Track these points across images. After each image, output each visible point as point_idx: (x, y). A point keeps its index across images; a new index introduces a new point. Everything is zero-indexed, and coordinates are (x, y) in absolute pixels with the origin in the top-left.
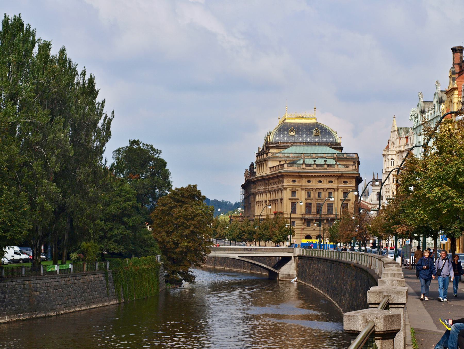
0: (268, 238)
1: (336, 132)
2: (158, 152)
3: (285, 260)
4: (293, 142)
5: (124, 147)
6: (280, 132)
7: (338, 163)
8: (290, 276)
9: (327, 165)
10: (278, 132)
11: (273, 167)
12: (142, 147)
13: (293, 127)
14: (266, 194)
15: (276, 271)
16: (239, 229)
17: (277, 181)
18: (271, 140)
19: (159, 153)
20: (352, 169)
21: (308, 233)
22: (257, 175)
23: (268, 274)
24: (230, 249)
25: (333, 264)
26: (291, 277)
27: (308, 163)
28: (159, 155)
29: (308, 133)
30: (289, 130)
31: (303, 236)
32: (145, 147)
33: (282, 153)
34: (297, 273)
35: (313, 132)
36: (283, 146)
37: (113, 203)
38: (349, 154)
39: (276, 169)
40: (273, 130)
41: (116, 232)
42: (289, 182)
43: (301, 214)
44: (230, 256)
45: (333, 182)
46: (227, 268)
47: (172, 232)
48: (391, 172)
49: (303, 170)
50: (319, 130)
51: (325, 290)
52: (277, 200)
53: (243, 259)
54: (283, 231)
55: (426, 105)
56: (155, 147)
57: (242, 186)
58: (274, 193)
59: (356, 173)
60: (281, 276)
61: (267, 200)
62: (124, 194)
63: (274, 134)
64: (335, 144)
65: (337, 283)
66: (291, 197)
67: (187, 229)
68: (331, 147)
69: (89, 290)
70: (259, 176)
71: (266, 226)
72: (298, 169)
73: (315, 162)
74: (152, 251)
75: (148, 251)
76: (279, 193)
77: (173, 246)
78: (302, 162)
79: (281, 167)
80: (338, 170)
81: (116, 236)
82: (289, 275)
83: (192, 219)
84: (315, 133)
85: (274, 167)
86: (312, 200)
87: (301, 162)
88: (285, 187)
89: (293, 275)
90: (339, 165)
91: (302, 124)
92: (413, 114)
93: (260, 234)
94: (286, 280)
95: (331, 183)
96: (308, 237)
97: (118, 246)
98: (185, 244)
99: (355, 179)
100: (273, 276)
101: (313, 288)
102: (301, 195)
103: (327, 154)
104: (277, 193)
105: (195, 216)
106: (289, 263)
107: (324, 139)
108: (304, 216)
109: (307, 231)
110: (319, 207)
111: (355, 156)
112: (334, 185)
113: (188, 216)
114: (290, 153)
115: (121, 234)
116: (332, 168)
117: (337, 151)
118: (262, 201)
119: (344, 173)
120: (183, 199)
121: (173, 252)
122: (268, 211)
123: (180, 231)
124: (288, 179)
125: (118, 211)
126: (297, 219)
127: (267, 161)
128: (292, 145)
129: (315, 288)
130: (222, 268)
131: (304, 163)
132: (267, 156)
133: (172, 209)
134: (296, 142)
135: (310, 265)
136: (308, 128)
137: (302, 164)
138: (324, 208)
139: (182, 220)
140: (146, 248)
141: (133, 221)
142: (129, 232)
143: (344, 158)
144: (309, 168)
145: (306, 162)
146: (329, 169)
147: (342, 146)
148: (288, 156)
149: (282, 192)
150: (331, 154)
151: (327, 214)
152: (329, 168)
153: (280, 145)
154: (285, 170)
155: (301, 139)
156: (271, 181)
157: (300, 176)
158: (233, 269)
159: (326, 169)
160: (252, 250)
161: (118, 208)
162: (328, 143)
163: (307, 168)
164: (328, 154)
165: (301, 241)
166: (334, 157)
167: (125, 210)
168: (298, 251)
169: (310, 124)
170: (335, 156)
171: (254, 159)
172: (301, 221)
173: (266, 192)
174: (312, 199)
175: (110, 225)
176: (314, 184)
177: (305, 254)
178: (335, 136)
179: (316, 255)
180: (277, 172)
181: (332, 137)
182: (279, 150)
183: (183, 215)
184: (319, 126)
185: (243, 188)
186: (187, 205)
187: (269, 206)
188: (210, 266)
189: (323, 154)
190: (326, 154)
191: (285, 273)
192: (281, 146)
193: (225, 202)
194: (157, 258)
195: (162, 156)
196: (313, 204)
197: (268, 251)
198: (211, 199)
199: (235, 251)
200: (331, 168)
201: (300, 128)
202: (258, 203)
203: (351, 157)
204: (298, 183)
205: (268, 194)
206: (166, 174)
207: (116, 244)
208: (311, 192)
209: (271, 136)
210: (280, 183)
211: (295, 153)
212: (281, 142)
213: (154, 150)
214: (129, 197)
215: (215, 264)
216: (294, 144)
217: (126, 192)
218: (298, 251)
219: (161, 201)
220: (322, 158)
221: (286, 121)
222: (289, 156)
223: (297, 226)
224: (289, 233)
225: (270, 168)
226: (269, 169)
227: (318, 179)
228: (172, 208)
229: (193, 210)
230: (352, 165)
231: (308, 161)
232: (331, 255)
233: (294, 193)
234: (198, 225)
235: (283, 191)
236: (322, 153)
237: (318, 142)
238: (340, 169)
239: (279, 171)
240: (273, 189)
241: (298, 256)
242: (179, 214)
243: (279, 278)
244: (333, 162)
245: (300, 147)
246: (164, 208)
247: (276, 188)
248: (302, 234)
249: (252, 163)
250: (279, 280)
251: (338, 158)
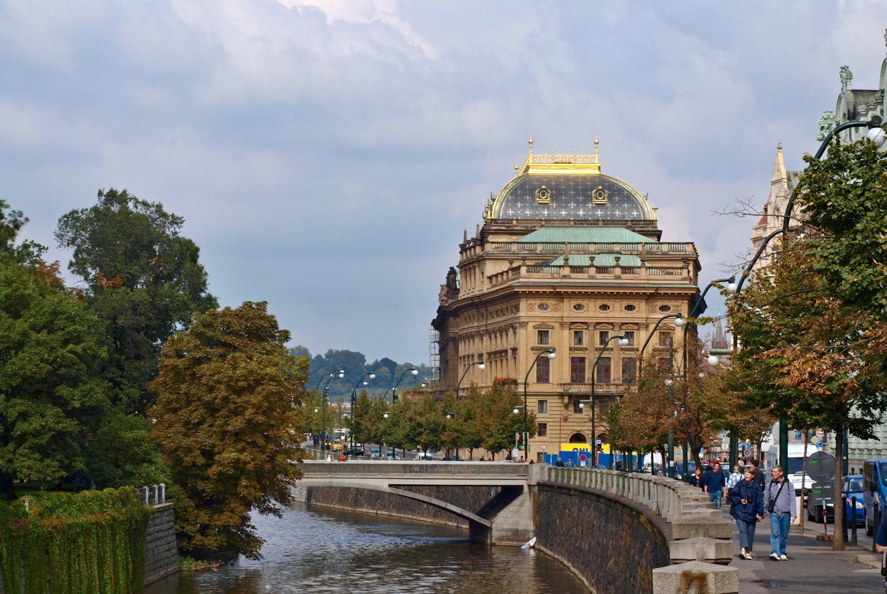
0: (473, 439)
2: (176, 221)
3: (510, 494)
4: (546, 220)
5: (86, 210)
6: (516, 198)
8: (519, 536)
9: (622, 268)
10: (510, 198)
11: (496, 276)
12: (134, 210)
13: (546, 185)
14: (482, 339)
15: (484, 522)
16: (411, 419)
17: (504, 306)
18: (496, 215)
19: (177, 224)
20: (679, 277)
21: (578, 428)
22: (462, 295)
23: (468, 527)
24: (369, 468)
25: (610, 509)
26: (522, 538)
27: (576, 264)
28: (177, 230)
29: (581, 198)
30: (537, 191)
31: (566, 436)
32: (141, 210)
33: (518, 243)
34: (536, 527)
35: (591, 196)
36: (523, 229)
37: (30, 347)
38: (673, 243)
39: (502, 278)
40: (501, 194)
41: (36, 423)
42: (532, 310)
43: (561, 384)
44: (368, 485)
45: (634, 307)
46: (384, 513)
47: (201, 423)
48: (768, 240)
49: (564, 280)
50: (606, 191)
51: (593, 578)
52: (506, 351)
53: (401, 492)
54: (507, 422)
55: (861, 99)
56: (168, 209)
58: (498, 335)
60: (495, 534)
61: (484, 352)
62: (60, 322)
64: (642, 223)
65: (616, 563)
66: (537, 345)
67: (236, 415)
68: (634, 231)
70: (466, 296)
71: (469, 411)
74: (145, 475)
75: (133, 474)
76: (509, 335)
77: (201, 460)
78: (562, 263)
80: (648, 280)
81: (36, 434)
82: (516, 532)
83: (251, 389)
84: (597, 199)
85: (499, 276)
86: (587, 352)
87: (560, 261)
88: (522, 320)
89: (526, 531)
90: (650, 268)
91: (567, 178)
92: (826, 125)
93: (457, 431)
94: (509, 543)
95: (631, 310)
96: (577, 438)
97: (41, 460)
98: (230, 455)
99: (688, 300)
100: (479, 532)
101: (568, 567)
102: (562, 339)
103: (623, 243)
104: (504, 334)
105: (258, 382)
106: (516, 502)
107: (617, 213)
108: (567, 387)
110: (603, 368)
111: (689, 248)
113: (240, 381)
114: (536, 243)
115: (50, 430)
116: (632, 275)
118: (473, 356)
119: (662, 286)
120: (229, 339)
121: (202, 477)
122: (486, 377)
123: (219, 422)
124: (529, 302)
125: (42, 368)
127: (482, 262)
128: (542, 226)
129: (572, 569)
130: (372, 511)
132: (483, 250)
133: (199, 365)
134: (553, 220)
135: (565, 508)
136: (580, 187)
137: (563, 266)
138: (614, 368)
139: (224, 393)
140: (129, 467)
141: (84, 396)
142: (73, 423)
143: (663, 253)
144: (580, 275)
145: (571, 263)
146: (627, 279)
147: (659, 229)
148: (531, 250)
149: (515, 332)
150: (632, 243)
151: (621, 382)
152: (625, 275)
154: (521, 280)
155: (563, 213)
156: (492, 309)
157: (558, 294)
158: (396, 515)
159: (619, 278)
160: (423, 469)
161: (42, 360)
162: (627, 221)
163: (574, 275)
164: (625, 243)
165: (560, 447)
166: (638, 251)
167: (61, 366)
168: (538, 474)
169: (584, 178)
170: (640, 247)
171: (455, 259)
172: (561, 401)
173: (482, 333)
174: (586, 349)
175: (20, 405)
176: (591, 311)
177: (553, 479)
178: (644, 206)
179: (577, 483)
180: (505, 285)
183: (225, 380)
184: (605, 182)
185: (436, 328)
186: (238, 354)
187: (480, 364)
188: (346, 508)
189: (613, 243)
190: (620, 243)
191: (505, 527)
192: (518, 228)
193: (428, 368)
195: (184, 233)
196: (589, 360)
197: (465, 472)
198: (399, 363)
199: (330, 471)
201: (563, 187)
202: (464, 361)
203: (679, 251)
205: (485, 338)
206: (197, 279)
207: (37, 456)
208: (584, 331)
209: (494, 206)
210: (512, 312)
211: (547, 243)
212: (517, 220)
213: (164, 215)
214: (75, 331)
215: (356, 503)
216: (548, 223)
217: (67, 319)
218: (539, 472)
219: (172, 345)
221: (531, 172)
222: (533, 250)
223: (551, 412)
224: (522, 428)
225: (490, 278)
226: (487, 281)
227: (600, 302)
228: (198, 361)
229: (253, 365)
230: (681, 268)
231: (577, 260)
232: (607, 483)
233: (543, 334)
234: (266, 404)
235: (517, 331)
236: (612, 241)
237: (604, 219)
238: (652, 277)
239: (509, 283)
240: (497, 326)
241: (539, 484)
242: (216, 378)
243: (491, 540)
244: (636, 262)
245: (560, 228)
246: (180, 363)
247: (503, 325)
248: (562, 432)
249: (452, 268)
250: (493, 545)
251: (649, 252)
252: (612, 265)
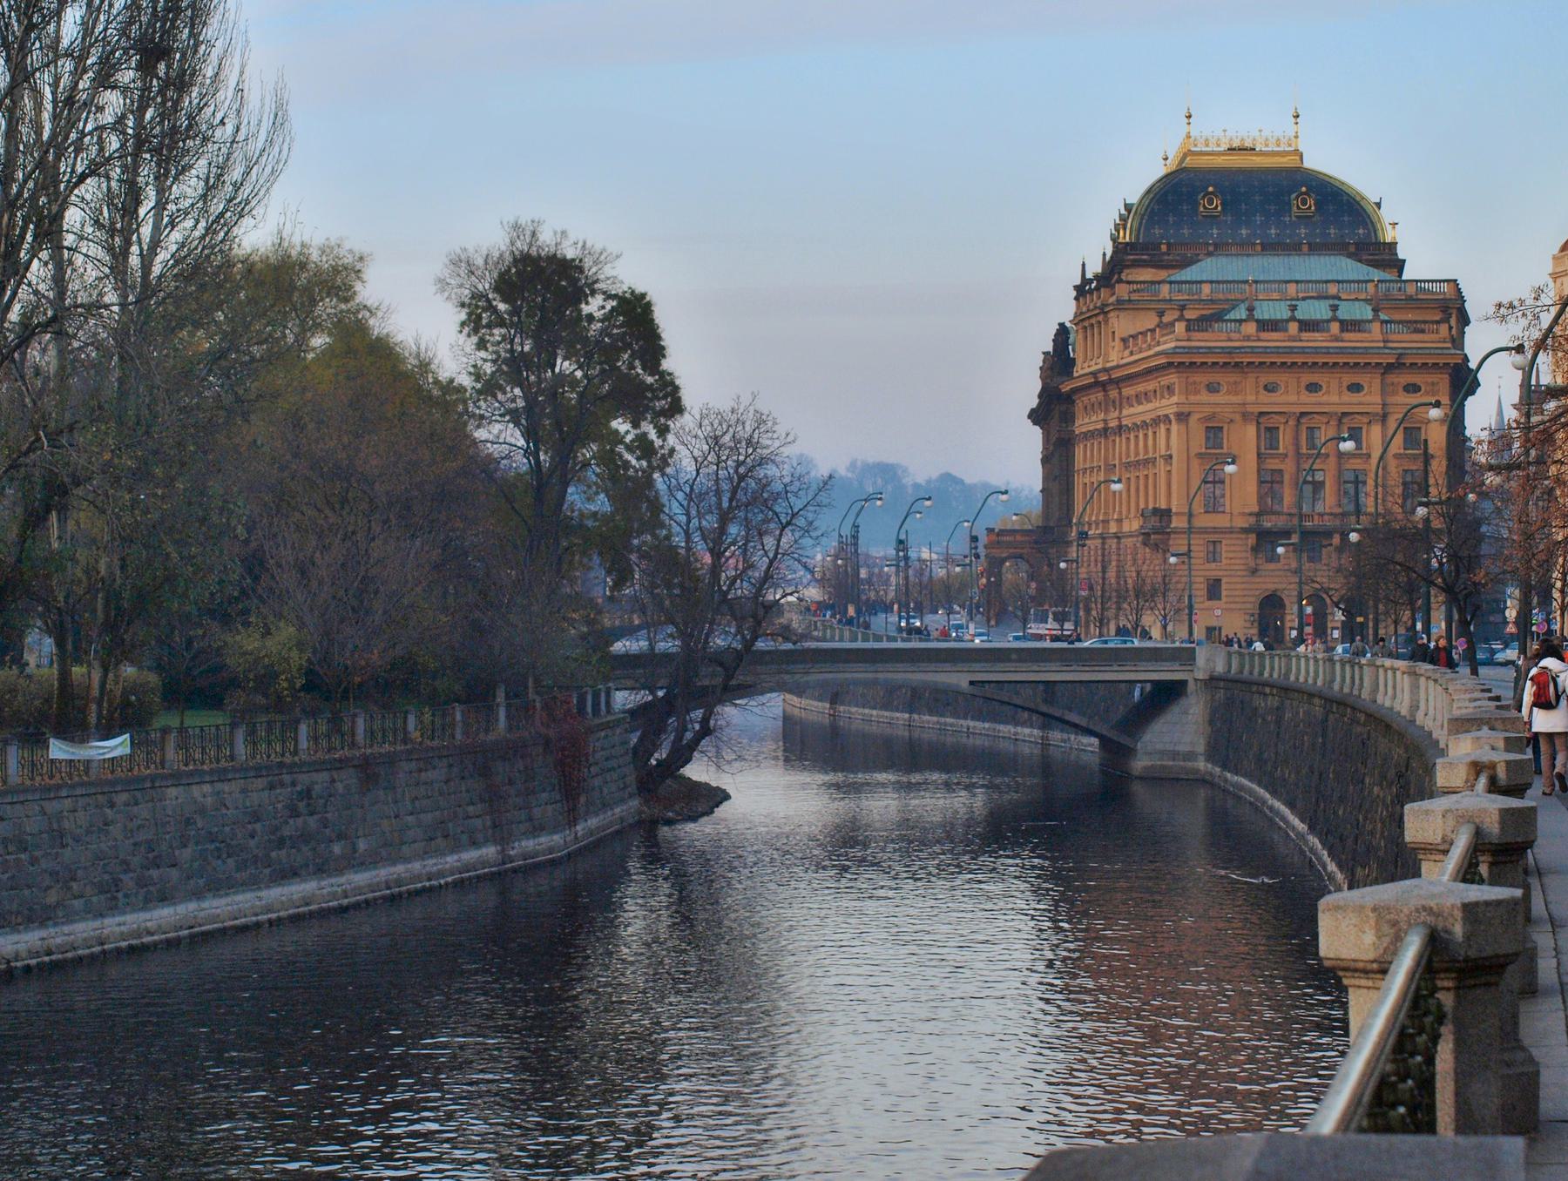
7: (1383, 316)
9: (1342, 322)
59: (1453, 351)
66: (1203, 450)
68: (1360, 261)
69: (185, 854)
73: (1293, 311)
79: (1163, 335)
87: (1241, 313)
90: (1387, 322)
117: (1382, 273)
126: (1230, 530)
137: (1245, 321)
144: (1274, 335)
145: (1258, 314)
146: (1353, 339)
153: (1164, 254)
171: (1066, 310)
176: (1290, 396)
181: (1365, 226)
194: (603, 695)
200: (1358, 336)
204: (1229, 392)
210: (1162, 397)
211: (1218, 282)
220: (1321, 297)
230: (1438, 322)
231: (1266, 311)
249: (1062, 325)
252: (1325, 317)
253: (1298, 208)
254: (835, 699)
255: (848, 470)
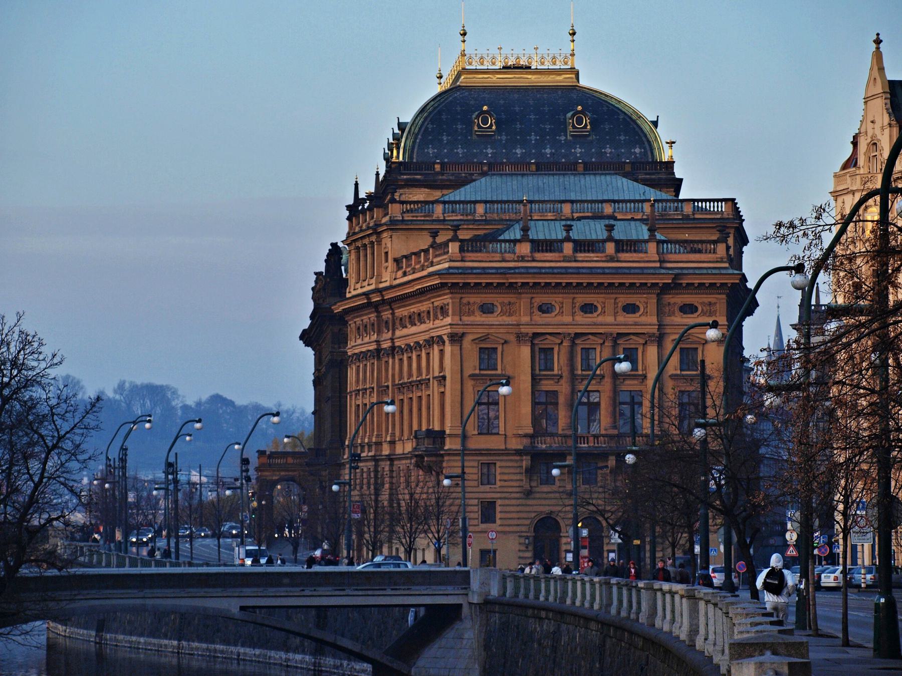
1: (653, 122)
7: (659, 236)
10: (430, 126)
20: (711, 256)
21: (547, 509)
57: (301, 338)
63: (417, 135)
68: (636, 180)
72: (504, 260)
79: (436, 256)
87: (515, 233)
90: (663, 242)
99: (728, 296)
107: (608, 150)
109: (544, 502)
112: (644, 319)
117: (658, 193)
126: (506, 452)
131: (525, 238)
136: (546, 109)
137: (519, 241)
144: (549, 256)
145: (532, 235)
156: (401, 312)
178: (652, 138)
182: (437, 194)
201: (517, 109)
210: (436, 318)
230: (715, 242)
249: (334, 245)
253: (574, 127)
254: (101, 628)
255: (115, 392)
